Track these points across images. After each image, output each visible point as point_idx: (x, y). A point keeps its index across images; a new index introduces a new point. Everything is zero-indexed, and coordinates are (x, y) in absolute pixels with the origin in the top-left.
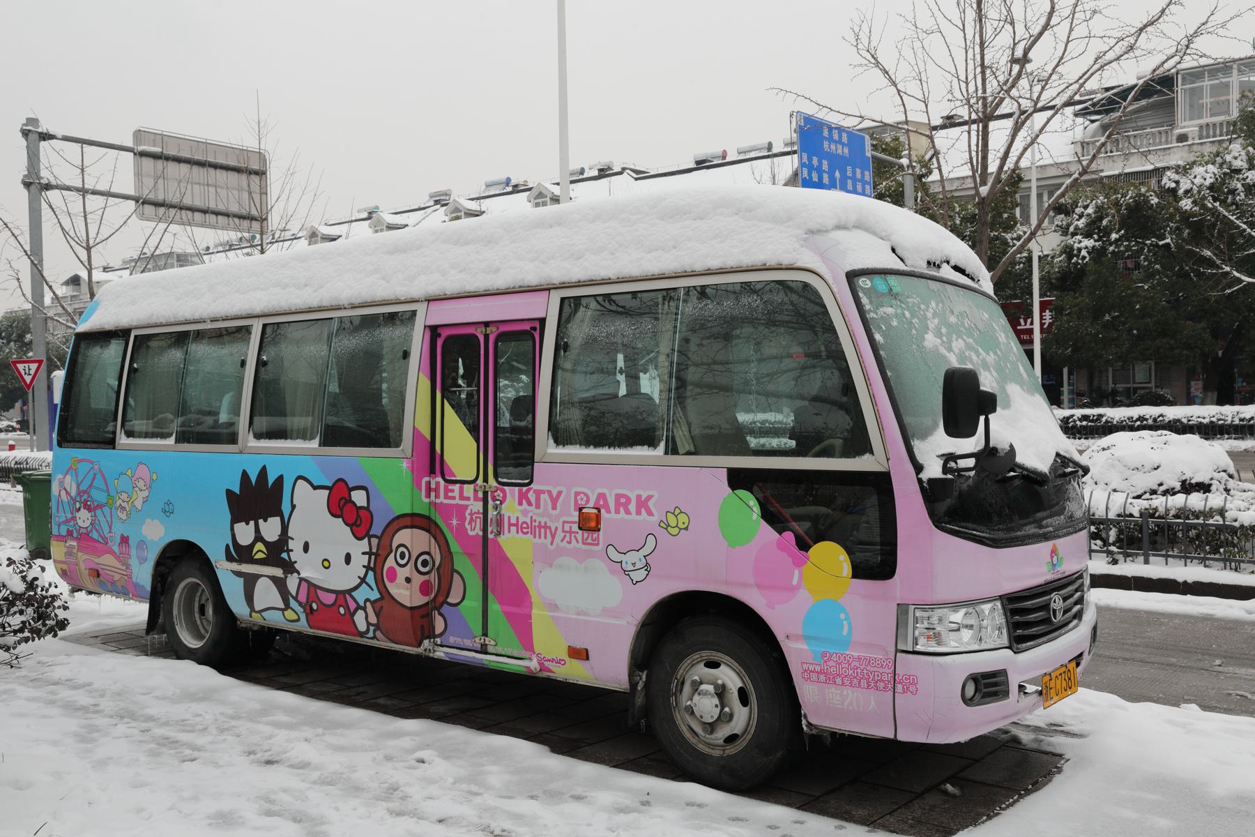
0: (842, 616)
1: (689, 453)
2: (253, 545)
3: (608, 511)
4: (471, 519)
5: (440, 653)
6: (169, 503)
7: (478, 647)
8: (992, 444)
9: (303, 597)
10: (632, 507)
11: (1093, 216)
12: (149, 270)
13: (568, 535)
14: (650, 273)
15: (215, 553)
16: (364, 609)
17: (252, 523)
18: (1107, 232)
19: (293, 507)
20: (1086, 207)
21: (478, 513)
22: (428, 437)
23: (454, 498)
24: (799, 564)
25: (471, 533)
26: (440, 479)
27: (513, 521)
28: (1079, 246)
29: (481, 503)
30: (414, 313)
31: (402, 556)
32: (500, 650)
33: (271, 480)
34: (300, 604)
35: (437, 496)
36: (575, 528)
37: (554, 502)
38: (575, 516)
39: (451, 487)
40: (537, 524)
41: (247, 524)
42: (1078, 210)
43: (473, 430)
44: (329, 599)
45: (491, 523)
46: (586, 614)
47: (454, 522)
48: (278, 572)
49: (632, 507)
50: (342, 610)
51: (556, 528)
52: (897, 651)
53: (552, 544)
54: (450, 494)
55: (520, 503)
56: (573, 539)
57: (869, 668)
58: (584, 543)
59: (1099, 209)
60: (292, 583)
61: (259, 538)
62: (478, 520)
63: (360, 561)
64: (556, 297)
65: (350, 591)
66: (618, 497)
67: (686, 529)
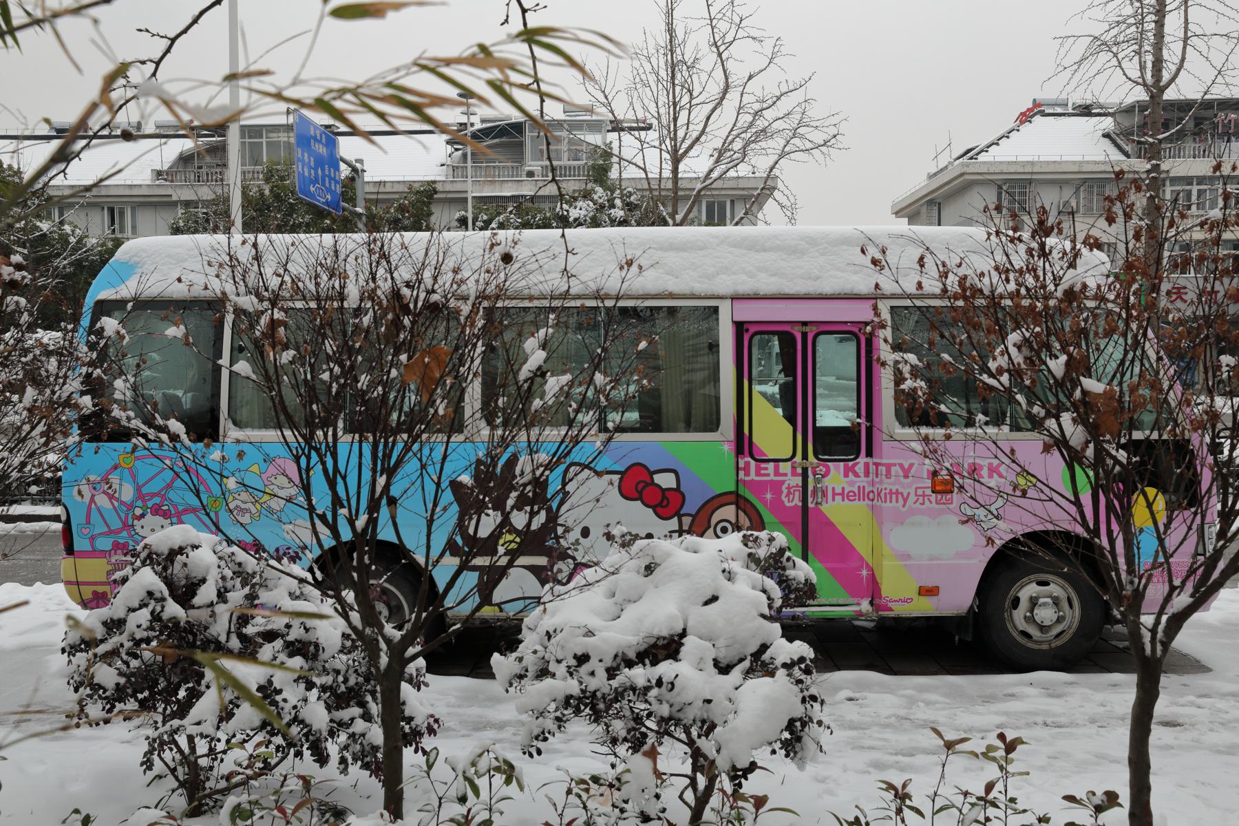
12: (692, 223)
13: (921, 498)
14: (751, 293)
21: (797, 486)
23: (768, 475)
26: (749, 459)
27: (838, 490)
29: (800, 478)
35: (747, 474)
36: (929, 492)
39: (763, 465)
40: (887, 491)
46: (938, 559)
47: (769, 496)
53: (904, 506)
54: (763, 472)
55: (846, 475)
58: (937, 503)
62: (797, 493)
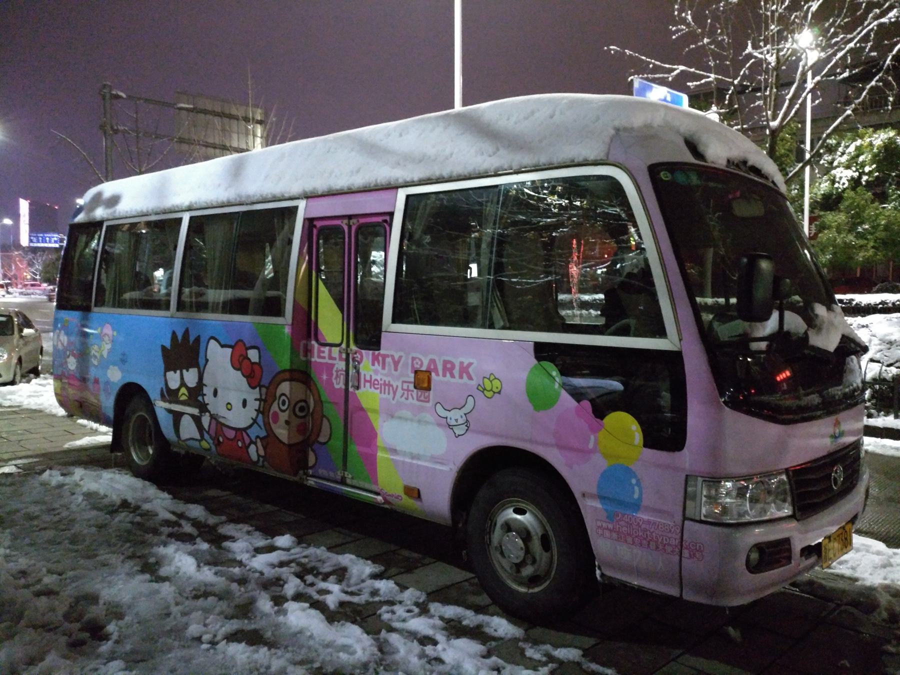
0: (634, 481)
1: (504, 328)
2: (178, 389)
3: (437, 375)
4: (337, 375)
5: (311, 482)
6: (124, 354)
7: (339, 478)
8: (786, 328)
9: (212, 432)
10: (456, 372)
11: (853, 154)
15: (154, 395)
16: (255, 443)
17: (178, 372)
18: (863, 165)
19: (207, 361)
20: (847, 147)
21: (342, 370)
22: (305, 306)
23: (324, 358)
24: (595, 430)
25: (337, 387)
27: (368, 378)
28: (841, 175)
30: (296, 208)
31: (284, 403)
32: (355, 482)
33: (192, 339)
34: (211, 437)
36: (411, 387)
37: (396, 363)
38: (411, 377)
39: (322, 349)
40: (382, 382)
41: (175, 372)
42: (840, 149)
43: (339, 303)
44: (231, 434)
45: (353, 379)
48: (195, 411)
49: (456, 372)
50: (240, 444)
51: (397, 386)
52: (685, 518)
53: (393, 399)
54: (322, 355)
55: (373, 364)
56: (410, 396)
57: (656, 532)
58: (418, 400)
59: (858, 148)
60: (206, 420)
61: (183, 384)
63: (253, 405)
64: (402, 194)
65: (245, 429)
66: (445, 363)
67: (499, 393)
